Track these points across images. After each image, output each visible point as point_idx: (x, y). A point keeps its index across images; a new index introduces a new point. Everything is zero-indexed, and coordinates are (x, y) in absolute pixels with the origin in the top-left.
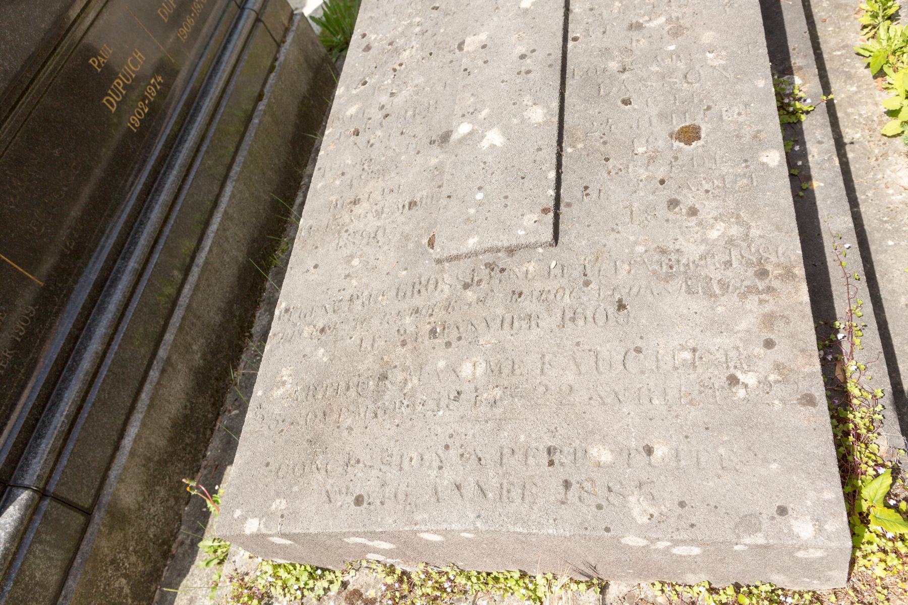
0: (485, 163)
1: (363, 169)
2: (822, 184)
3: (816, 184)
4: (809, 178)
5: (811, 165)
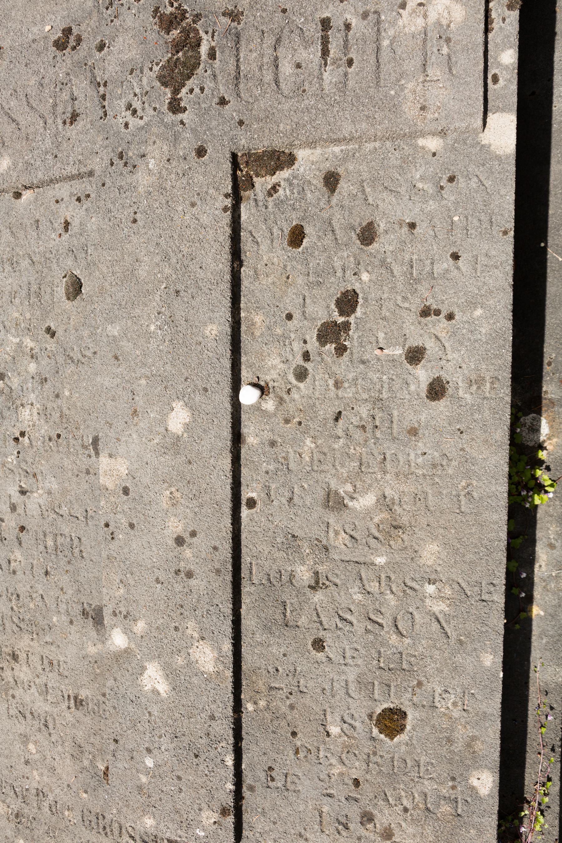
2: (542, 613)
3: (536, 611)
4: (530, 599)
5: (536, 579)
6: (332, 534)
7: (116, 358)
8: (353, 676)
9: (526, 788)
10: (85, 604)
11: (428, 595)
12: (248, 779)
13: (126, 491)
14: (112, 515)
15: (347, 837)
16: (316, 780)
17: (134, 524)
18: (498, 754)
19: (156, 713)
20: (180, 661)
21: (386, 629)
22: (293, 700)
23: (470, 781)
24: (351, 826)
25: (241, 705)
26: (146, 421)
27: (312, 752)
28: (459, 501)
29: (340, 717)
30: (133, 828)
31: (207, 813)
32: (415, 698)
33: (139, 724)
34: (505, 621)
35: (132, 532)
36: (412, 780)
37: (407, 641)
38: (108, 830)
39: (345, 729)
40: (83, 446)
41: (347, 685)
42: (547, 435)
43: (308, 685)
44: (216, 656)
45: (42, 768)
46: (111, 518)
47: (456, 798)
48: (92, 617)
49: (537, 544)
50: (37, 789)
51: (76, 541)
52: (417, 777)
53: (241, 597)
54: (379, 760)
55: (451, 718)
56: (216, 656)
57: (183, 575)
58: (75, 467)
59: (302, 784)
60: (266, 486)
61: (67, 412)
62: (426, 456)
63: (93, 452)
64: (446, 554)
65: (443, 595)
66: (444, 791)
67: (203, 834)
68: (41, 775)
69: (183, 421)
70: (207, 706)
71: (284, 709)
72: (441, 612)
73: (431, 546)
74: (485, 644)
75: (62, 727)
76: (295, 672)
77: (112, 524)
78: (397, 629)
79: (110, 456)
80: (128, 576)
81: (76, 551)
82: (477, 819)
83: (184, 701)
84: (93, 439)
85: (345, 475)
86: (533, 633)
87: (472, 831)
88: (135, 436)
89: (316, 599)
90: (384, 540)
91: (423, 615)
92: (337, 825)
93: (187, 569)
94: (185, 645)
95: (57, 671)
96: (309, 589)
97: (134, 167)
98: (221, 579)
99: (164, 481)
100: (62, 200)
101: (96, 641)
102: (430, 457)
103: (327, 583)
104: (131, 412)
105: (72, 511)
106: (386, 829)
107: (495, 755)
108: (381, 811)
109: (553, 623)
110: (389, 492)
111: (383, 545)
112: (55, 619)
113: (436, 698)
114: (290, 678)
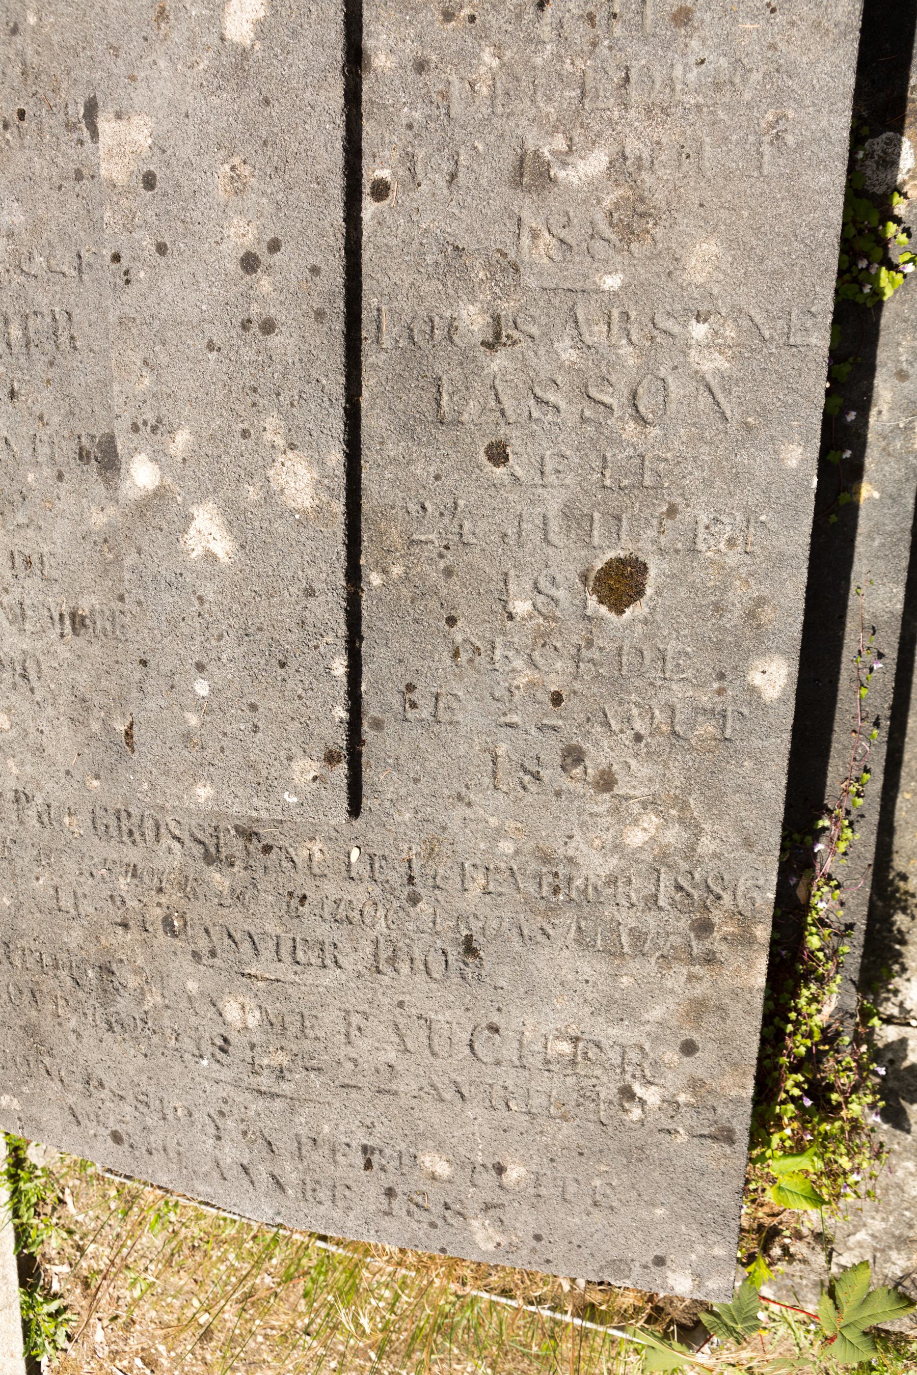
2: (876, 495)
3: (868, 492)
6: (526, 240)
8: (556, 506)
9: (828, 789)
10: (83, 439)
11: (694, 342)
12: (371, 709)
13: (149, 181)
14: (125, 236)
15: (538, 793)
16: (489, 699)
17: (165, 245)
18: (799, 627)
19: (211, 597)
20: (252, 493)
21: (617, 413)
22: (450, 558)
23: (749, 678)
24: (545, 774)
25: (360, 576)
26: (184, 27)
27: (482, 650)
28: (761, 154)
29: (531, 582)
30: (178, 822)
31: (301, 763)
32: (663, 540)
33: (182, 624)
34: (828, 385)
35: (162, 261)
36: (651, 684)
37: (655, 432)
38: (137, 836)
39: (539, 605)
40: (67, 125)
41: (545, 524)
42: (909, 170)
43: (477, 531)
44: (316, 476)
45: (21, 753)
46: (122, 242)
47: (725, 711)
48: (96, 460)
49: (877, 374)
50: (16, 791)
51: (62, 319)
52: (661, 678)
53: (360, 374)
54: (597, 655)
55: (723, 568)
56: (316, 476)
57: (255, 328)
58: (55, 171)
59: (464, 709)
60: (407, 154)
61: (36, 60)
62: (703, 66)
63: (86, 134)
64: (730, 259)
65: (720, 341)
66: (705, 699)
67: (295, 800)
68: (22, 763)
69: (253, 16)
70: (300, 573)
71: (435, 576)
72: (717, 371)
73: (705, 246)
74: (791, 427)
75: (51, 672)
76: (456, 509)
77: (125, 255)
78: (637, 411)
79: (118, 116)
80: (157, 349)
81: (64, 339)
82: (756, 743)
83: (260, 568)
84: (86, 106)
85: (553, 118)
86: (859, 531)
87: (746, 763)
88: (162, 64)
89: (494, 367)
90: (621, 240)
91: (684, 381)
92: (521, 774)
93: (264, 316)
94: (260, 463)
95: (39, 572)
96: (482, 349)
98: (325, 329)
99: (220, 146)
101: (104, 501)
102: (711, 67)
103: (516, 335)
104: (153, 14)
105: (53, 262)
106: (603, 772)
107: (793, 629)
108: (596, 743)
109: (894, 510)
110: (633, 146)
111: (619, 251)
112: (31, 477)
113: (700, 535)
114: (446, 520)
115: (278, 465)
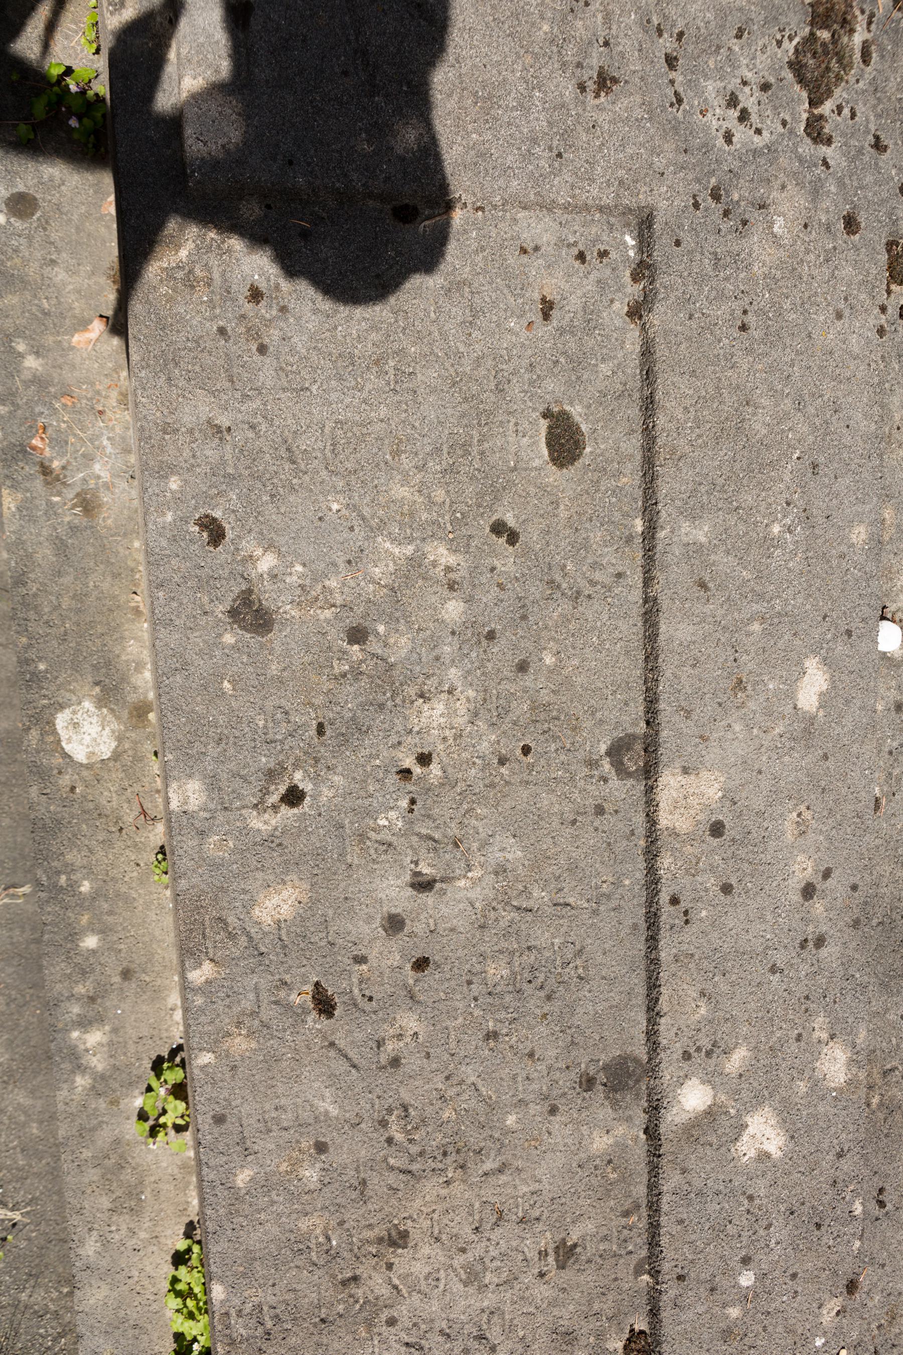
0: (751, 1198)
1: (390, 1141)
7: (703, 585)
13: (717, 829)
14: (686, 881)
79: (686, 771)
88: (737, 727)
97: (745, 223)
100: (537, 249)
115: (823, 1056)
